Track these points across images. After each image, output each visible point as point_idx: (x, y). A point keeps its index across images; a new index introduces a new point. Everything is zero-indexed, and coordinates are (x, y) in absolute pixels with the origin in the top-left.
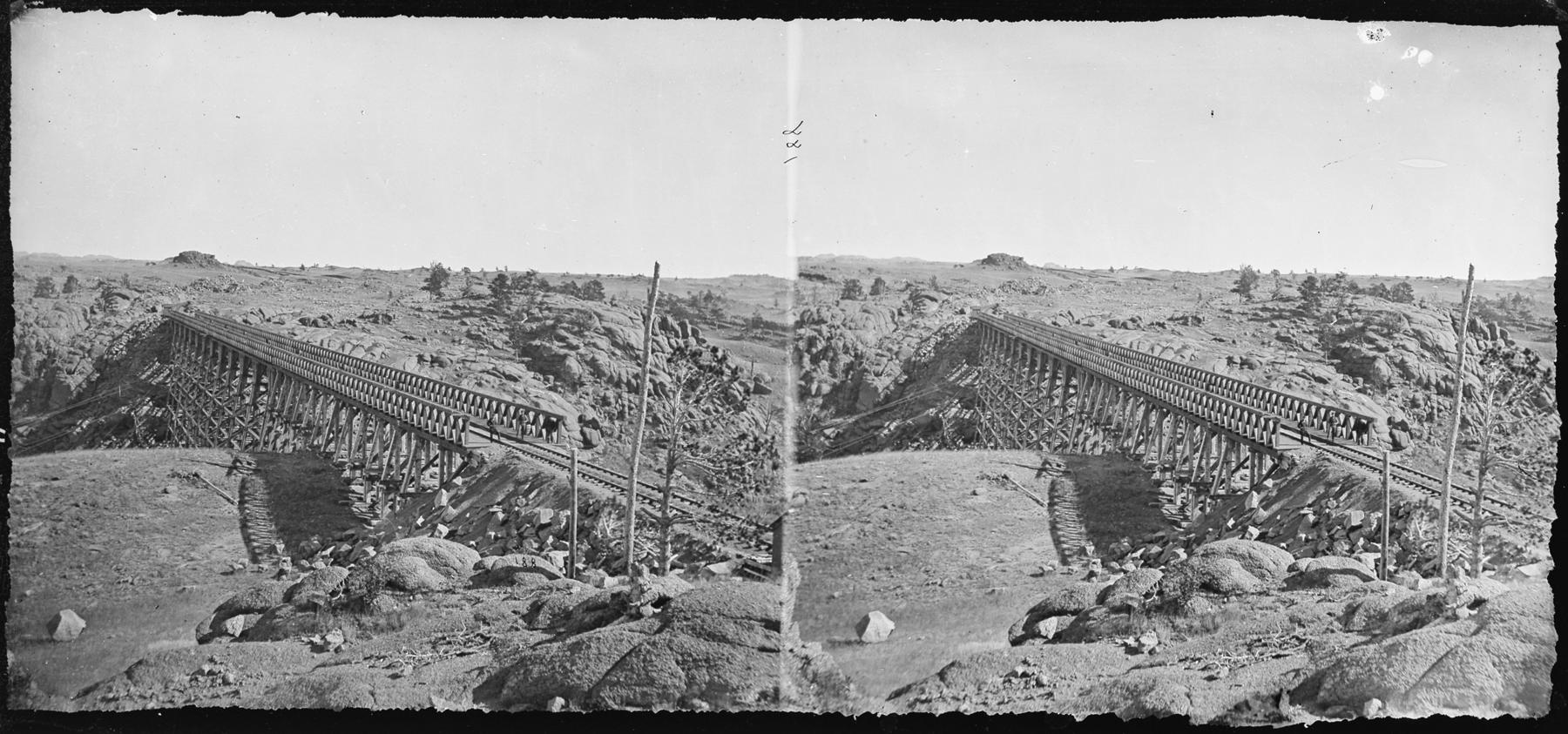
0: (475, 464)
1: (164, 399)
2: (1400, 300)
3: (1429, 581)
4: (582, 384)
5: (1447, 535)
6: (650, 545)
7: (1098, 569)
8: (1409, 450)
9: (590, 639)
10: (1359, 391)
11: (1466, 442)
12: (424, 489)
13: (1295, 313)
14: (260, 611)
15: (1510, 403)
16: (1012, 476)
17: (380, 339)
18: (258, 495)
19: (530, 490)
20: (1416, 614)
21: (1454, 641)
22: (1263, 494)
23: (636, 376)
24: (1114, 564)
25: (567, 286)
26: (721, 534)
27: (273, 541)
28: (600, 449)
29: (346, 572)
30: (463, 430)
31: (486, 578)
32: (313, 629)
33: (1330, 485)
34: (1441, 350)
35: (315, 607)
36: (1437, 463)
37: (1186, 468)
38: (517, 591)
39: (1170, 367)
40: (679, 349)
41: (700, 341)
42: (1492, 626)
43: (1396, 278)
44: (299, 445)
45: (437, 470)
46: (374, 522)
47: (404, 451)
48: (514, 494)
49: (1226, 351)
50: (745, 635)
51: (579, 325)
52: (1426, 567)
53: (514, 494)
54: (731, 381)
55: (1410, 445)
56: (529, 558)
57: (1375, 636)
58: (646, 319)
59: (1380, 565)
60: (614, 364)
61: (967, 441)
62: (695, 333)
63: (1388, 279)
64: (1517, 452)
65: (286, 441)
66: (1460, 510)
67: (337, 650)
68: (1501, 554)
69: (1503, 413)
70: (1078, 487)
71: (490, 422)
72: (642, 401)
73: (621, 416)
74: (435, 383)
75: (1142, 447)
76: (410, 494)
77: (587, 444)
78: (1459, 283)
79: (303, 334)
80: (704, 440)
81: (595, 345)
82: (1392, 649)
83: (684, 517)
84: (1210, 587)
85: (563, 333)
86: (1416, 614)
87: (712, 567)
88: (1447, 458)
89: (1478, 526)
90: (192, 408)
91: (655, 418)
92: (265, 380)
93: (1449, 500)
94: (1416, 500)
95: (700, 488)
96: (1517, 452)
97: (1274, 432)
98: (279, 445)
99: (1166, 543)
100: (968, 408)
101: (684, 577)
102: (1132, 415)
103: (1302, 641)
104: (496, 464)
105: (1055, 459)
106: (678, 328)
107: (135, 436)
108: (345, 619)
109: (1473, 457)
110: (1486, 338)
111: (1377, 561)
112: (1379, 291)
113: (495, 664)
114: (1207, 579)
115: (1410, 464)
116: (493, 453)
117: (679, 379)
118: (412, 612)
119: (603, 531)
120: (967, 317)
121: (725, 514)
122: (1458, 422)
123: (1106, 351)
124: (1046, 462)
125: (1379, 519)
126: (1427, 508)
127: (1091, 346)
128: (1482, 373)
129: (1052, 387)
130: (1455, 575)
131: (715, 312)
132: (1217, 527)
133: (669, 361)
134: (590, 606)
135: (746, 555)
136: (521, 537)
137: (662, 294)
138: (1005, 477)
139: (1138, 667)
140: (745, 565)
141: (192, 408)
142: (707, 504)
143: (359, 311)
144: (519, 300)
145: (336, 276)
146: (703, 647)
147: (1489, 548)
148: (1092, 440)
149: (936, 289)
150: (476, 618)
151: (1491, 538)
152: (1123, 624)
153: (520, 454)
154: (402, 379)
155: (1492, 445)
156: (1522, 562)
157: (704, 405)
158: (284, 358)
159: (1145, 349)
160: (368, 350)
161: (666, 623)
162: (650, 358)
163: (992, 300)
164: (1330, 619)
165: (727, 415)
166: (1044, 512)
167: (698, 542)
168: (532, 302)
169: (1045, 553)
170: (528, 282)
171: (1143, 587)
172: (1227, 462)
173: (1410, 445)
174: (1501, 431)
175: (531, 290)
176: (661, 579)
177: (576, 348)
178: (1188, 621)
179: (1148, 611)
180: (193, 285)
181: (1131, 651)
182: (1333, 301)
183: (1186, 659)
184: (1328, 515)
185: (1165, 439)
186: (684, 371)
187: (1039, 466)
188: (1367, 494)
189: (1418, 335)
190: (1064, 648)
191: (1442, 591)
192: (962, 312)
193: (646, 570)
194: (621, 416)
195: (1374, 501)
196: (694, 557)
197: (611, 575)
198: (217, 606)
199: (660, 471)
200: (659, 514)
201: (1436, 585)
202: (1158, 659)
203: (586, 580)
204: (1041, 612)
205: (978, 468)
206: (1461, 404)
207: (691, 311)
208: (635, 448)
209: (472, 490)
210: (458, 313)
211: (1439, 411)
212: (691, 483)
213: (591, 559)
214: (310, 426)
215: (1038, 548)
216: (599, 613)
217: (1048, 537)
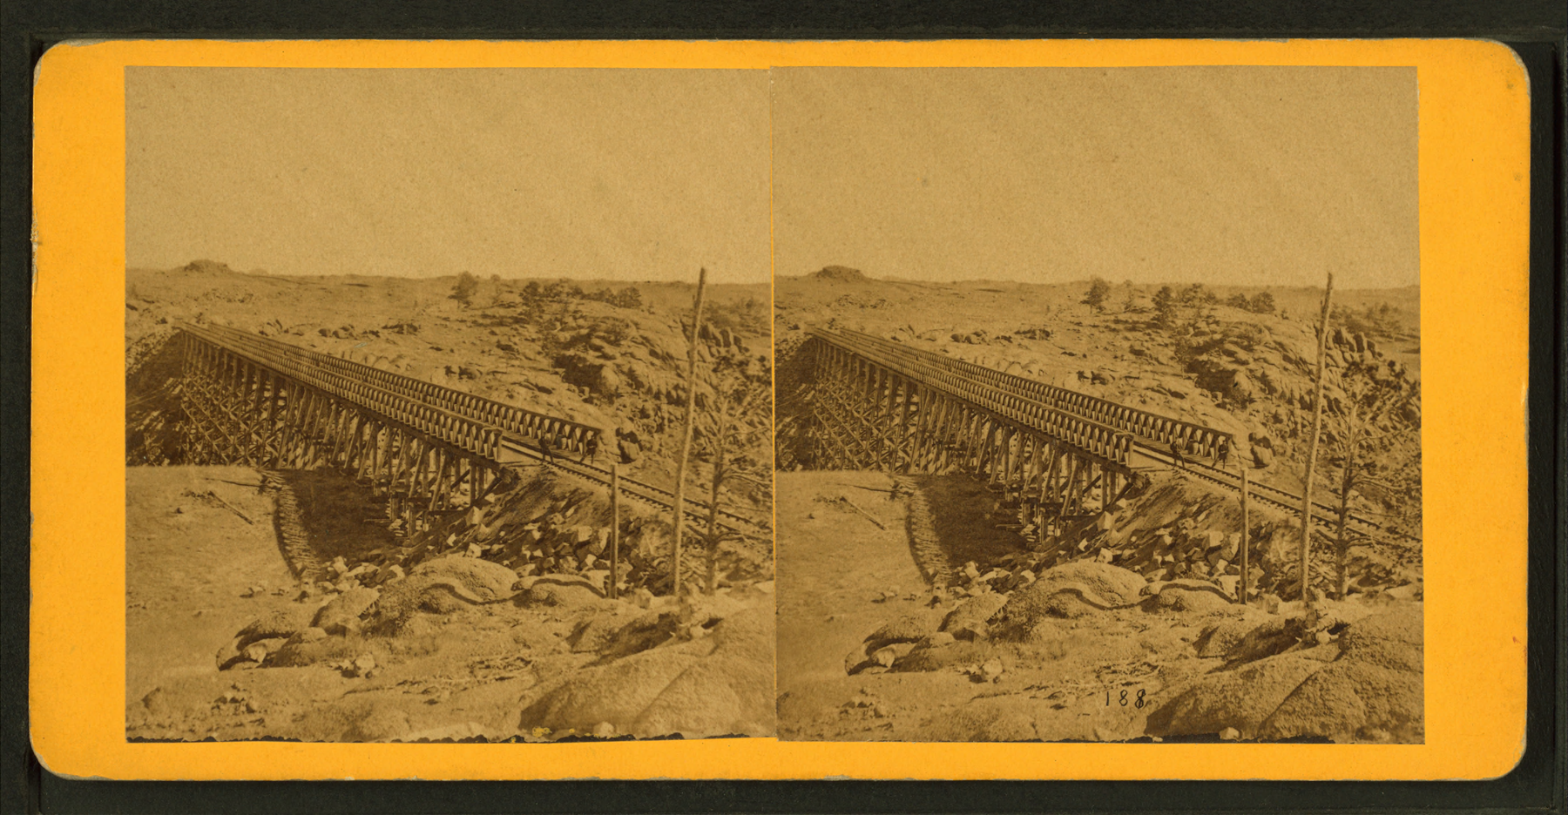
0: (508, 480)
5: (679, 551)
13: (1149, 325)
14: (913, 640)
21: (1315, 666)
23: (1310, 392)
28: (639, 463)
34: (672, 358)
36: (668, 475)
40: (1354, 363)
42: (729, 645)
43: (622, 283)
47: (433, 467)
49: (444, 359)
53: (552, 510)
58: (1319, 332)
62: (737, 341)
63: (1248, 290)
66: (693, 524)
67: (368, 675)
68: (737, 569)
69: (737, 423)
74: (1097, 401)
78: (689, 287)
79: (956, 352)
80: (1382, 459)
82: (1249, 676)
86: (1273, 639)
87: (1392, 592)
88: (679, 470)
91: (1330, 436)
93: (682, 515)
95: (1378, 509)
96: (753, 464)
97: (1127, 449)
102: (345, 428)
103: (528, 663)
104: (1161, 485)
106: (720, 337)
109: (707, 470)
110: (718, 344)
112: (1238, 302)
117: (1354, 395)
120: (168, 326)
121: (1405, 536)
122: (690, 432)
126: (658, 523)
128: (715, 382)
129: (893, 405)
130: (688, 592)
133: (715, 371)
134: (1263, 634)
136: (1189, 561)
142: (1386, 525)
143: (1016, 326)
146: (1383, 675)
147: (724, 564)
151: (1357, 560)
155: (727, 456)
157: (1383, 420)
158: (304, 371)
159: (357, 359)
161: (1344, 651)
162: (1325, 373)
163: (828, 314)
164: (1182, 644)
167: (1377, 565)
172: (1078, 481)
173: (640, 458)
174: (736, 442)
175: (1196, 302)
177: (1244, 363)
180: (206, 295)
182: (1190, 312)
183: (404, 682)
185: (1012, 458)
191: (676, 609)
193: (1321, 594)
194: (1294, 433)
199: (1335, 491)
200: (1335, 537)
201: (668, 603)
202: (376, 683)
206: (692, 415)
208: (1308, 467)
209: (510, 506)
210: (488, 321)
211: (670, 421)
214: (331, 442)
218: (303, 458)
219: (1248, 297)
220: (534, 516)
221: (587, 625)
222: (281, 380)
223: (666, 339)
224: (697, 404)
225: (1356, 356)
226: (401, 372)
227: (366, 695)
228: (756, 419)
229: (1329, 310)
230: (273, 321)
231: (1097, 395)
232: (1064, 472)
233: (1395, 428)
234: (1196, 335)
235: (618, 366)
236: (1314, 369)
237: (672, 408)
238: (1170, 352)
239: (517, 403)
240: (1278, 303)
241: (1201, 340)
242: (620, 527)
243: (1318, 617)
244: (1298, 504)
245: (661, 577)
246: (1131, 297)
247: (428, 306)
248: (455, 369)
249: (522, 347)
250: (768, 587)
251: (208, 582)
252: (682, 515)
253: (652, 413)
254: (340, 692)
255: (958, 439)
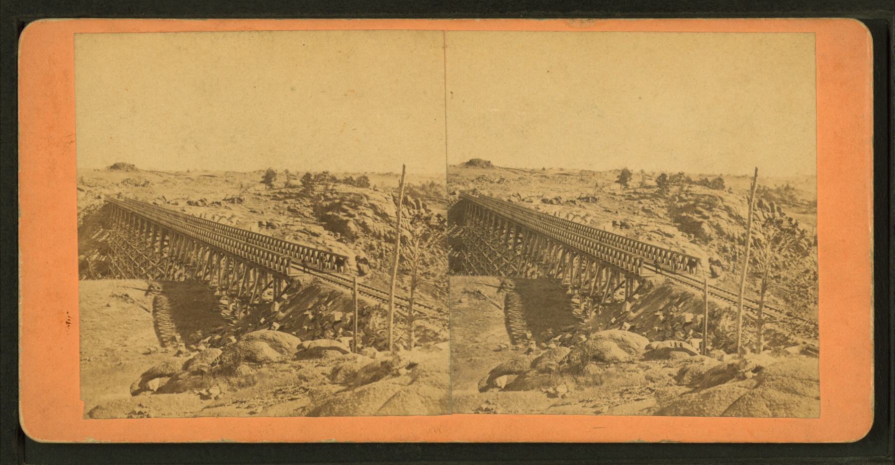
0: (647, 286)
1: (106, 251)
2: (362, 186)
3: (383, 353)
4: (358, 237)
5: (392, 325)
6: (751, 335)
7: (183, 349)
8: (721, 278)
9: (715, 392)
10: (338, 241)
11: (403, 270)
12: (616, 301)
13: (653, 195)
15: (429, 247)
16: (483, 291)
17: (236, 213)
18: (164, 307)
19: (327, 302)
20: (374, 373)
21: (398, 388)
22: (633, 303)
23: (744, 235)
24: (193, 346)
25: (702, 181)
26: (794, 329)
27: (525, 332)
29: (220, 352)
30: (640, 266)
31: (652, 354)
32: (549, 384)
33: (673, 298)
35: (550, 371)
36: (385, 283)
37: (587, 287)
38: (671, 362)
39: (224, 229)
40: (769, 219)
41: (782, 214)
42: (421, 379)
44: (541, 274)
45: (624, 290)
46: (586, 321)
48: (319, 303)
49: (257, 218)
50: (807, 390)
51: (710, 204)
52: (380, 345)
53: (319, 303)
54: (801, 238)
55: (722, 275)
56: (678, 343)
57: (696, 388)
58: (750, 201)
59: (352, 344)
60: (730, 227)
61: (103, 275)
64: (434, 275)
65: (534, 272)
66: (400, 310)
67: (563, 397)
69: (425, 253)
70: (170, 301)
71: (656, 262)
72: (746, 250)
73: (734, 258)
74: (623, 238)
75: (208, 276)
76: (608, 304)
77: (714, 275)
78: (397, 176)
80: (783, 273)
81: (364, 214)
82: (360, 394)
83: (772, 319)
84: (252, 359)
85: (700, 209)
86: (374, 373)
87: (789, 349)
88: (392, 280)
89: (411, 320)
90: (477, 252)
92: (521, 235)
93: (393, 305)
94: (724, 307)
95: (781, 302)
96: (434, 275)
98: (176, 276)
99: (223, 334)
100: (104, 255)
101: (772, 354)
102: (555, 255)
105: (157, 285)
106: (414, 203)
107: (89, 273)
108: (568, 378)
109: (407, 279)
110: (413, 208)
111: (350, 341)
113: (312, 405)
114: (248, 354)
115: (370, 283)
116: (306, 279)
117: (769, 237)
118: (608, 375)
119: (723, 327)
121: (796, 318)
122: (398, 258)
123: (186, 220)
124: (151, 286)
125: (351, 317)
126: (380, 310)
127: (531, 214)
128: (412, 228)
129: (154, 241)
130: (398, 349)
131: (791, 197)
132: (254, 323)
133: (763, 226)
134: (715, 372)
135: (809, 342)
136: (674, 330)
137: (759, 186)
138: (127, 295)
139: (208, 407)
140: (808, 348)
141: (477, 252)
142: (786, 312)
143: (578, 195)
144: (674, 189)
145: (565, 175)
147: (418, 333)
148: (178, 272)
149: (83, 183)
150: (647, 378)
152: (199, 381)
153: (673, 281)
154: (603, 236)
155: (419, 271)
156: (788, 345)
157: (785, 252)
159: (209, 218)
160: (583, 218)
161: (760, 382)
162: (752, 224)
164: (323, 376)
165: (797, 259)
166: (150, 315)
167: (780, 334)
168: (681, 190)
169: (502, 337)
170: (680, 179)
171: (211, 360)
172: (260, 284)
174: (424, 263)
176: (757, 356)
177: (707, 218)
178: (237, 379)
179: (214, 374)
181: (203, 397)
183: (583, 401)
184: (321, 315)
185: (575, 270)
186: (772, 232)
187: (499, 285)
188: (344, 302)
189: (373, 207)
190: (510, 393)
191: (390, 359)
192: (99, 197)
193: (748, 349)
195: (348, 306)
196: (778, 343)
197: (728, 353)
198: (490, 370)
199: (757, 292)
200: (756, 317)
201: (387, 355)
202: (220, 402)
203: (365, 354)
204: (149, 376)
205: (110, 291)
206: (399, 248)
207: (777, 196)
208: (742, 277)
209: (645, 302)
211: (387, 252)
212: (775, 299)
213: (716, 344)
214: (195, 264)
215: (147, 337)
216: (720, 376)
217: (152, 331)
218: (180, 274)
219: (355, 178)
220: (661, 308)
221: (687, 370)
222: (520, 228)
223: (384, 205)
224: (401, 242)
225: (770, 214)
226: (588, 224)
227: (215, 409)
228: (435, 250)
229: (756, 189)
230: (161, 197)
231: (269, 235)
232: (604, 278)
233: (791, 256)
234: (325, 200)
235: (357, 220)
236: (746, 221)
237: (387, 245)
238: (665, 211)
239: (654, 243)
240: (727, 183)
241: (683, 204)
242: (709, 315)
243: (400, 360)
244: (736, 299)
245: (382, 340)
246: (644, 179)
247: (604, 187)
248: (265, 223)
249: (656, 210)
250: (445, 346)
251: (476, 342)
252: (393, 305)
253: (729, 249)
254: (200, 407)
255: (545, 259)
